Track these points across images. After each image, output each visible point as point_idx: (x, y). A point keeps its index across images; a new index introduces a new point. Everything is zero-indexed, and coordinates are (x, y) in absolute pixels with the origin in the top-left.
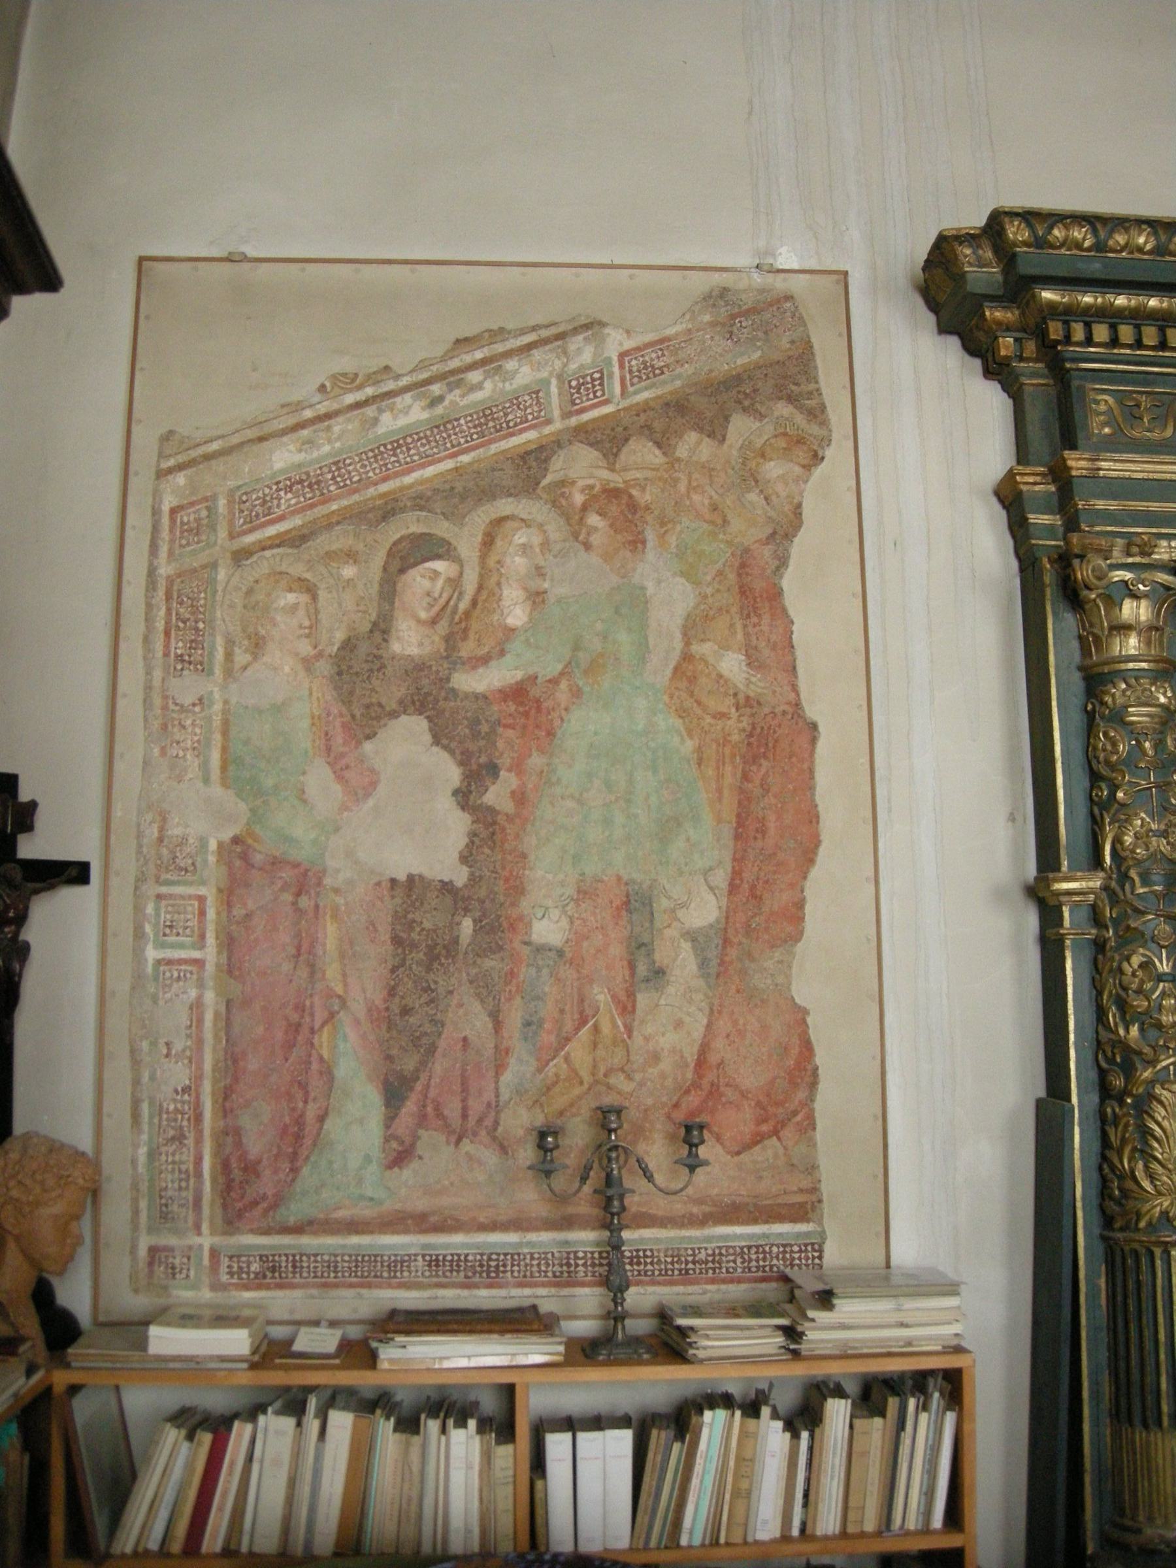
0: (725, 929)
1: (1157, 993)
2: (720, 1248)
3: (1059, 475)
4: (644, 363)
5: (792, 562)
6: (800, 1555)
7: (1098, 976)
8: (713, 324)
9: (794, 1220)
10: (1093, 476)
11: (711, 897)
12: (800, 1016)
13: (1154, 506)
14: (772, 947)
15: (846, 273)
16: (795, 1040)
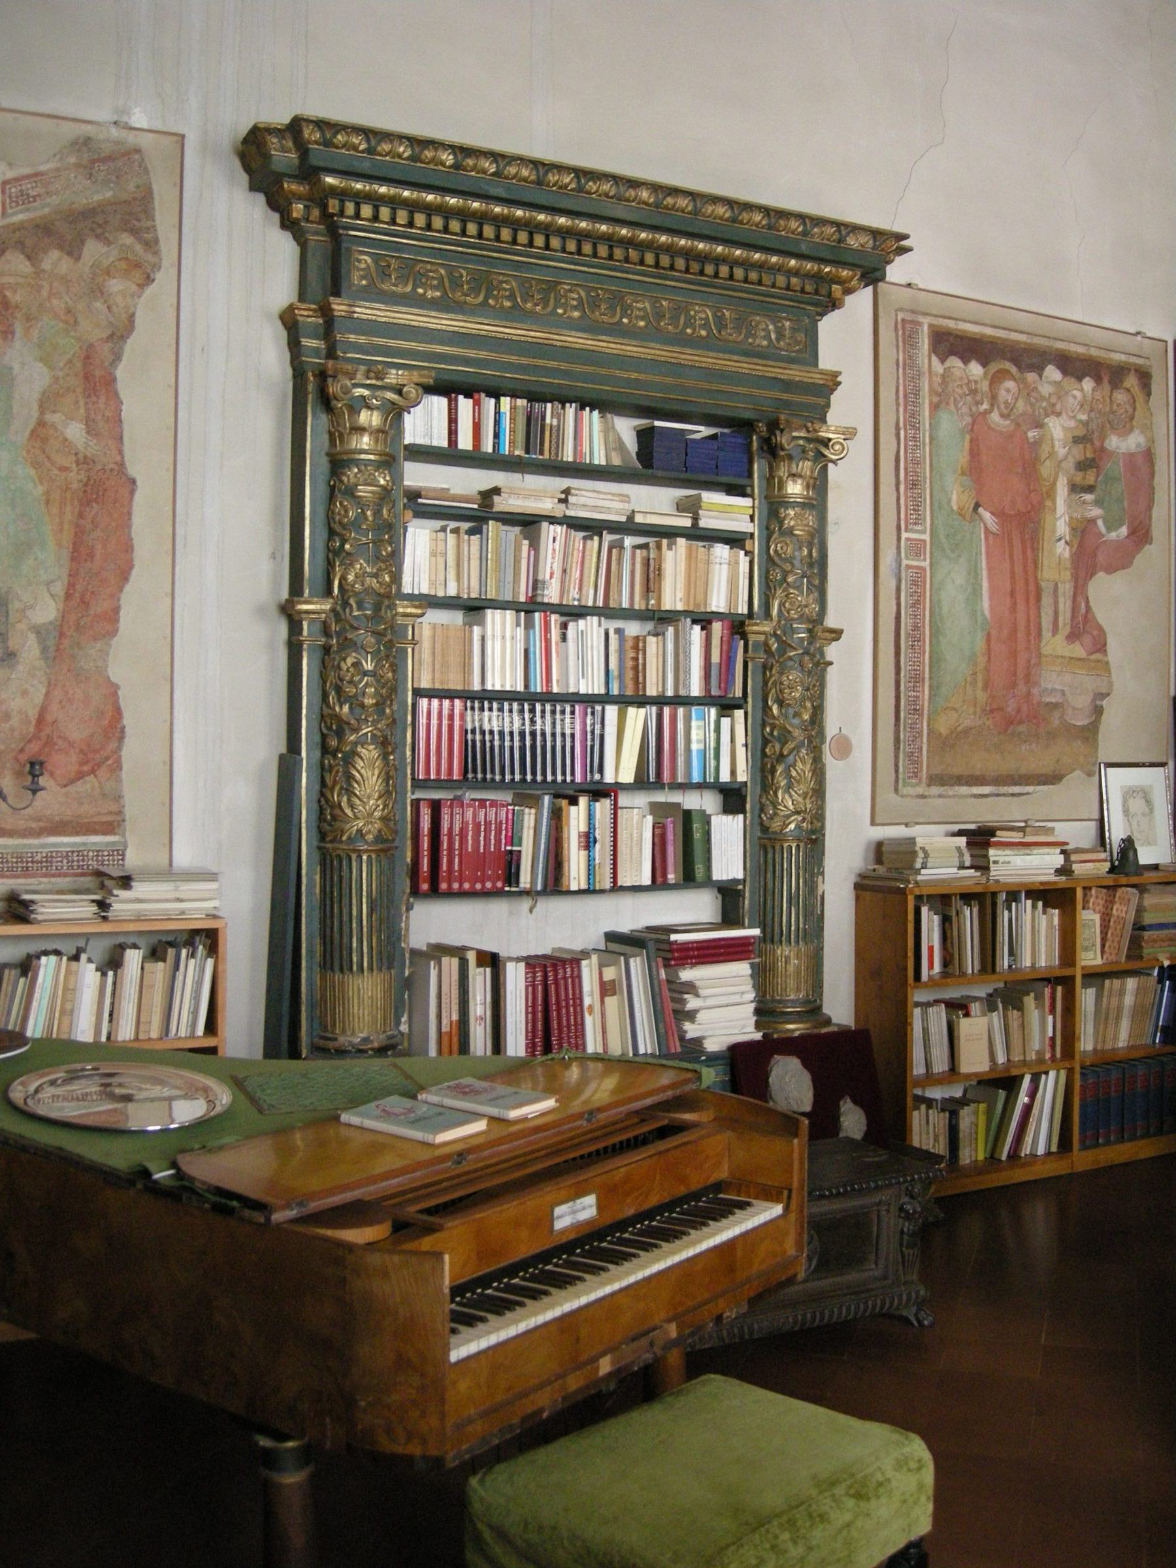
4: (21, 191)
5: (125, 358)
8: (78, 166)
9: (105, 833)
10: (350, 317)
12: (113, 691)
13: (392, 343)
15: (183, 136)
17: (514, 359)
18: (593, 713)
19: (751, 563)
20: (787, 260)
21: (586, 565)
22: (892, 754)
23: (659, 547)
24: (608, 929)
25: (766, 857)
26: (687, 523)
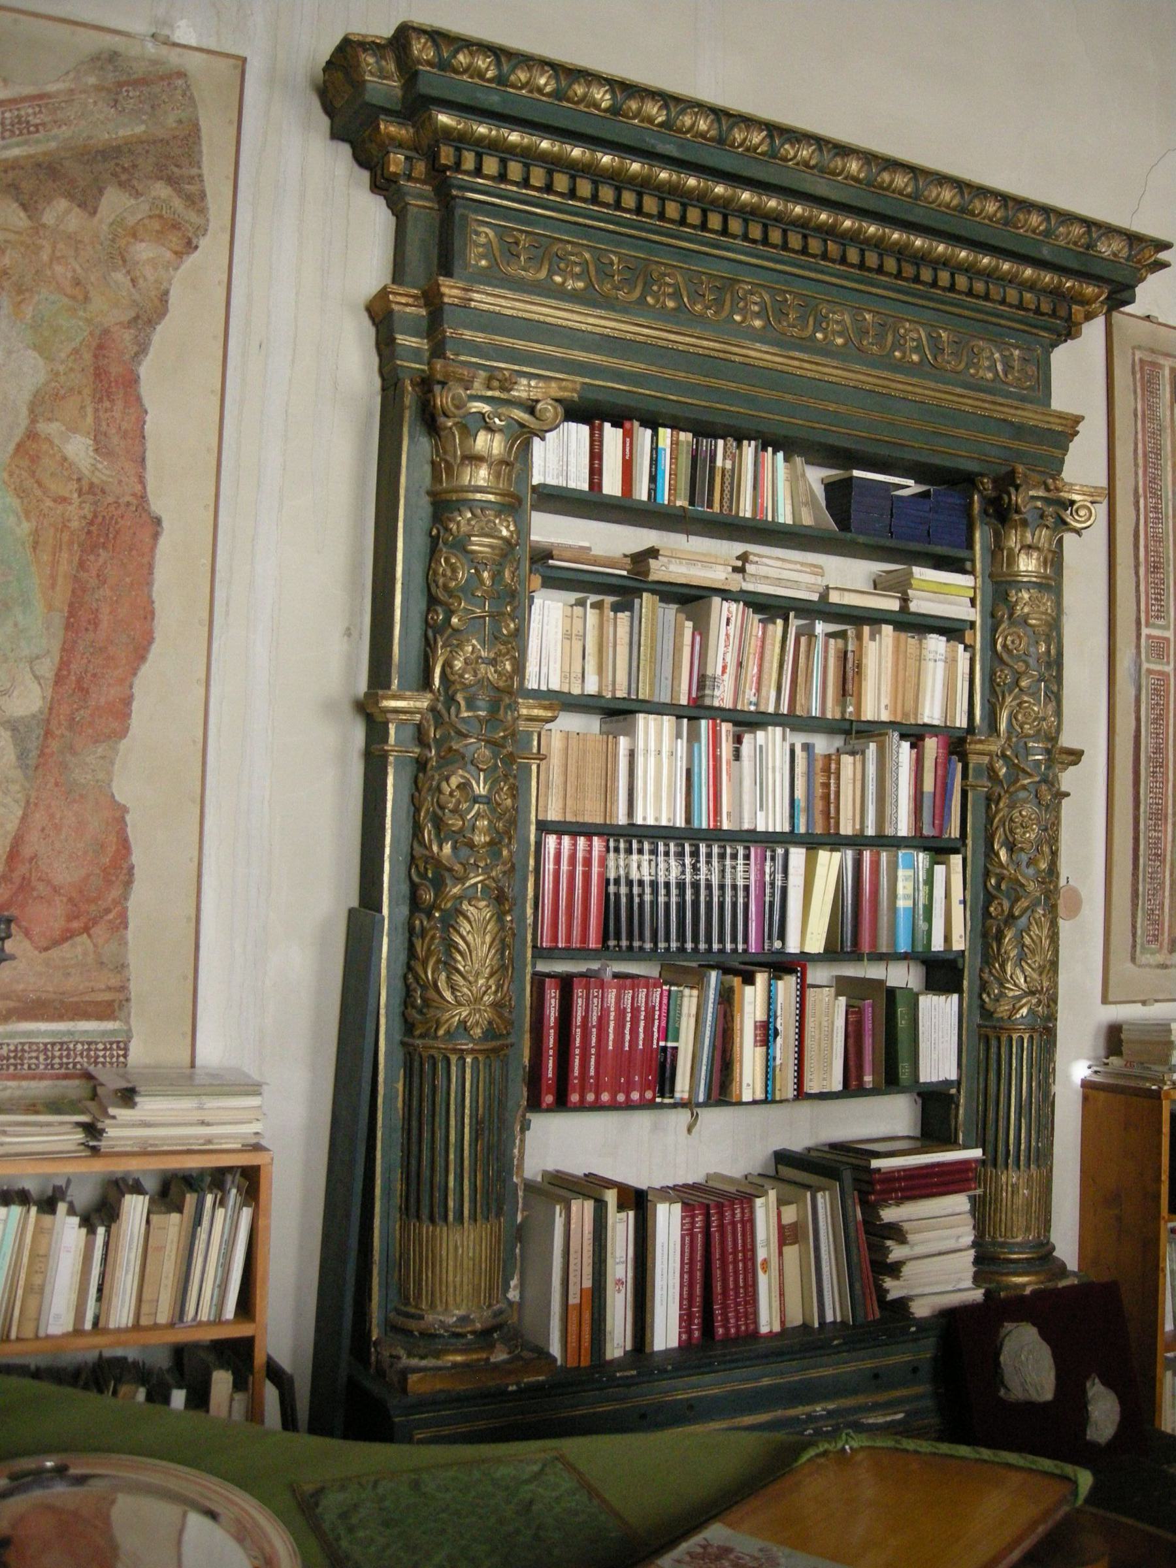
0: (48, 721)
1: (472, 814)
2: (23, 1044)
3: (432, 299)
4: (19, 117)
6: (95, 1347)
7: (417, 794)
8: (98, 88)
9: (100, 1018)
10: (465, 305)
11: (35, 687)
12: (118, 816)
13: (520, 344)
14: (96, 741)
15: (244, 60)
16: (113, 838)
17: (681, 375)
18: (773, 859)
19: (972, 661)
20: (1021, 268)
21: (767, 657)
22: (1129, 913)
23: (859, 637)
24: (778, 1148)
25: (987, 1050)
26: (894, 605)
